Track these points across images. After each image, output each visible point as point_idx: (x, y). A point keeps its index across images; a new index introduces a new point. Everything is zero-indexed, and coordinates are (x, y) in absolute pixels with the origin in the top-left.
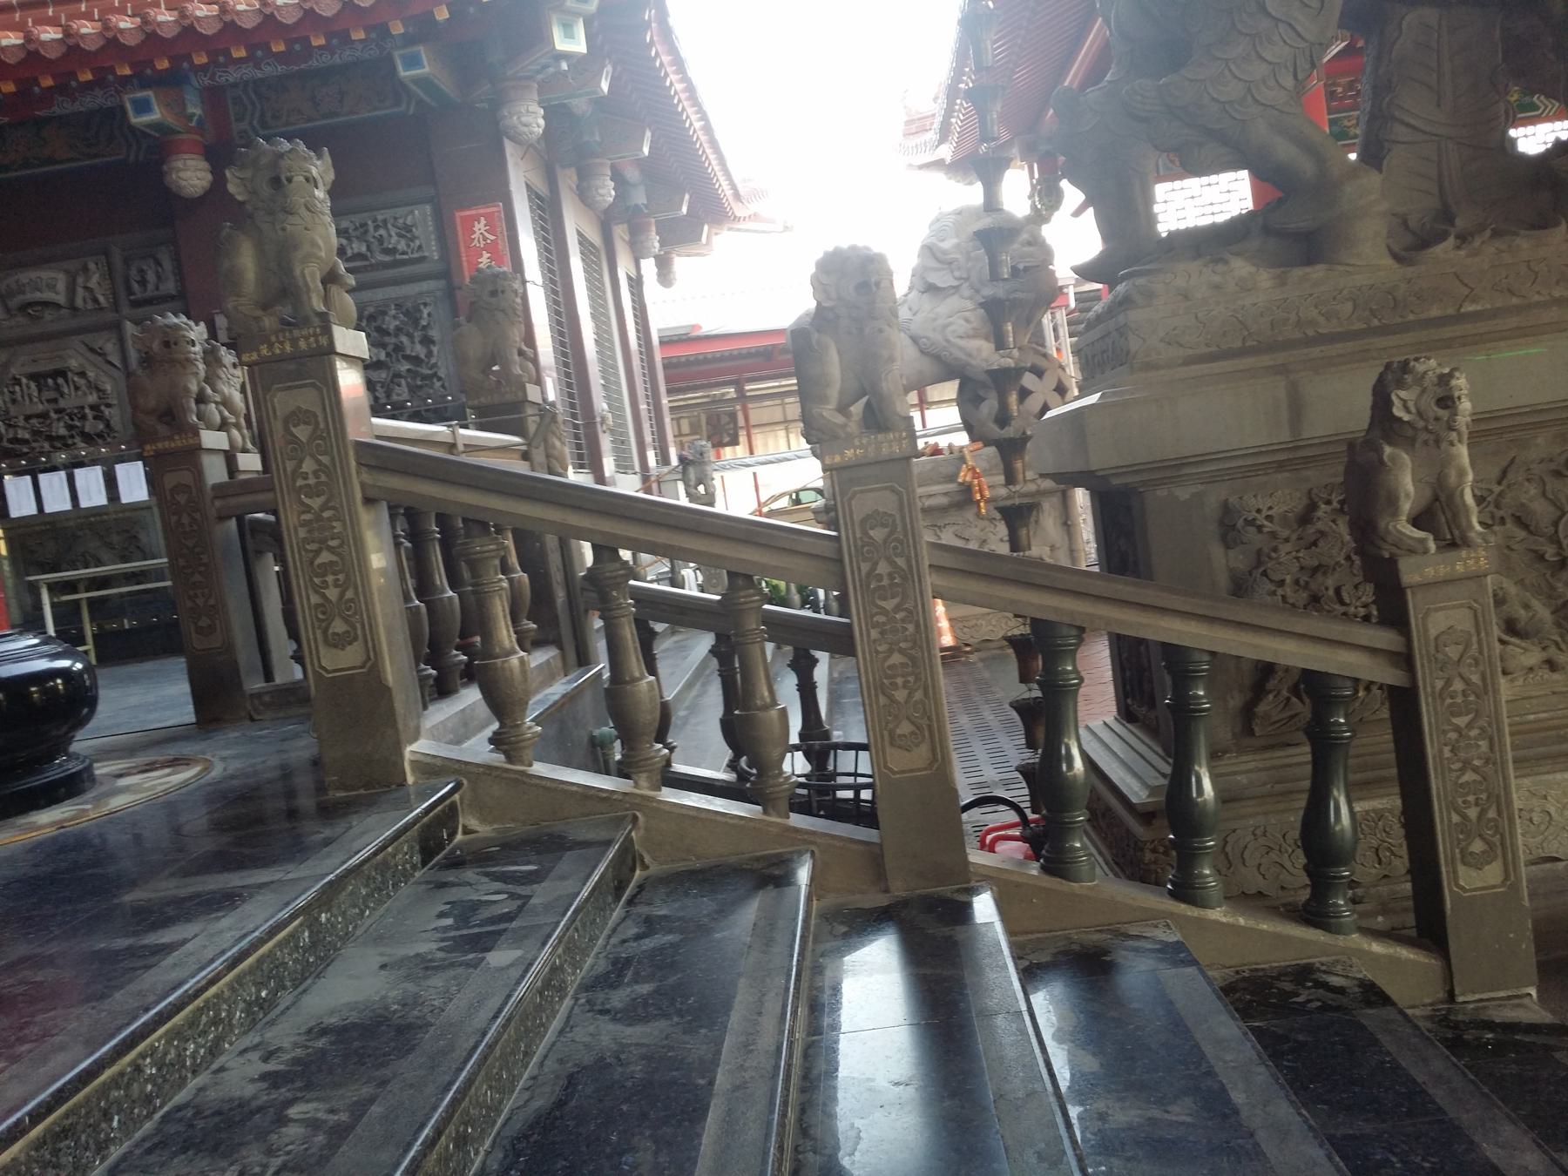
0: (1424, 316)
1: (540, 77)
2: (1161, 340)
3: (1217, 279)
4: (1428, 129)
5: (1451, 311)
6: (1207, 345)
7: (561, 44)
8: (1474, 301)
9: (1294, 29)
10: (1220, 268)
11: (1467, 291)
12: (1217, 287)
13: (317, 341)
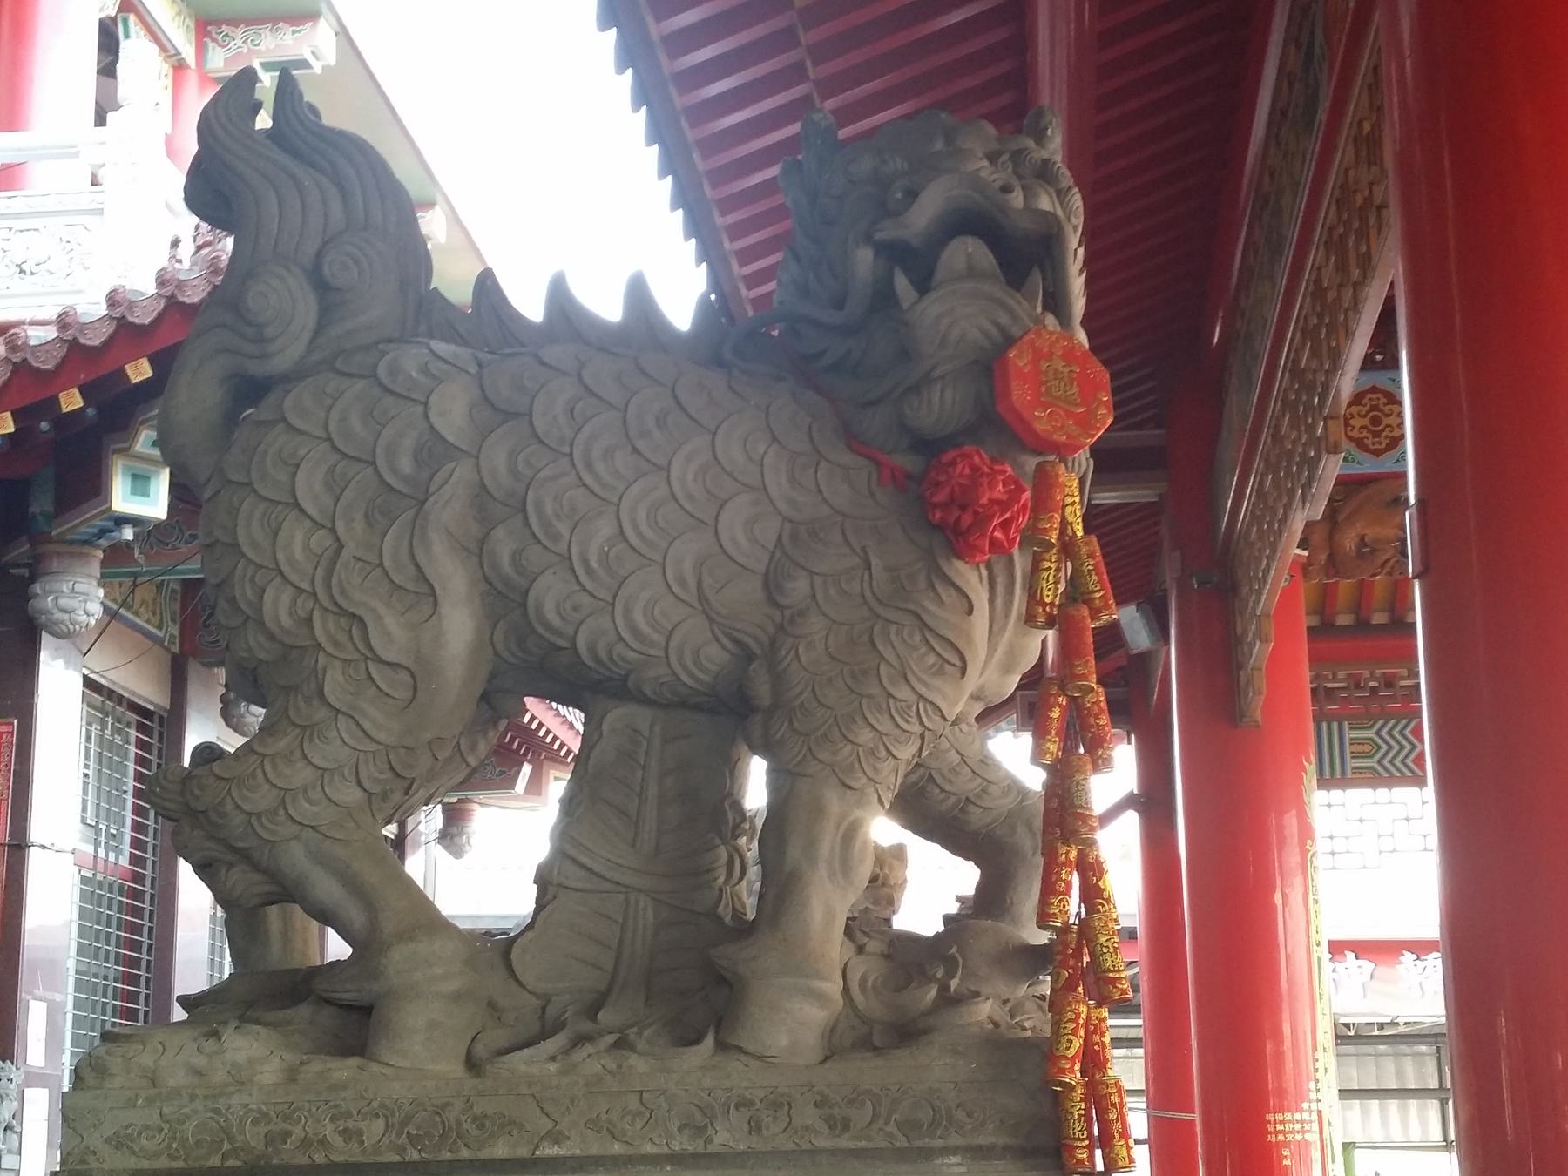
0: (485, 1154)
1: (103, 542)
2: (108, 1141)
3: (200, 1061)
4: (609, 875)
5: (523, 1152)
6: (172, 1157)
7: (123, 500)
8: (557, 1142)
9: (358, 725)
10: (210, 1045)
11: (550, 1125)
12: (198, 1073)
13: (1070, 1020)
